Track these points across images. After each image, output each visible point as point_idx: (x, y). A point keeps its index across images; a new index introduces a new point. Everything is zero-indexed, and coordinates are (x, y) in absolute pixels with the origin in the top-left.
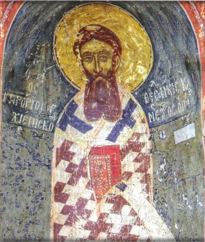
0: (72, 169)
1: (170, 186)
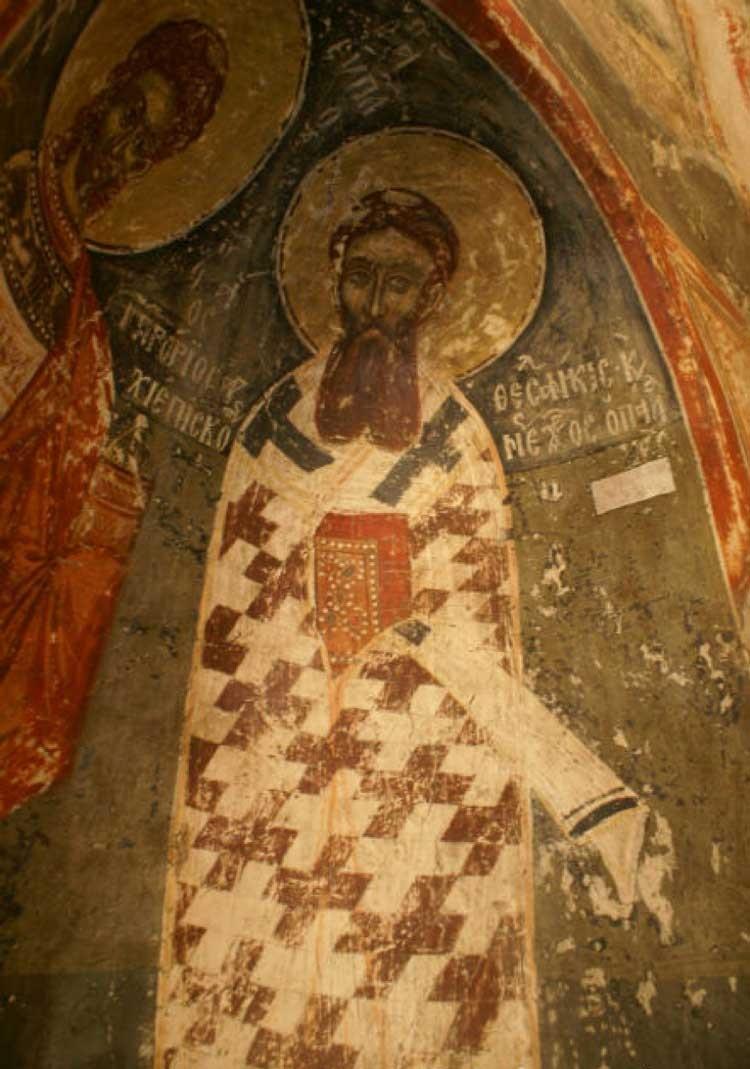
0: (265, 570)
1: (588, 624)
